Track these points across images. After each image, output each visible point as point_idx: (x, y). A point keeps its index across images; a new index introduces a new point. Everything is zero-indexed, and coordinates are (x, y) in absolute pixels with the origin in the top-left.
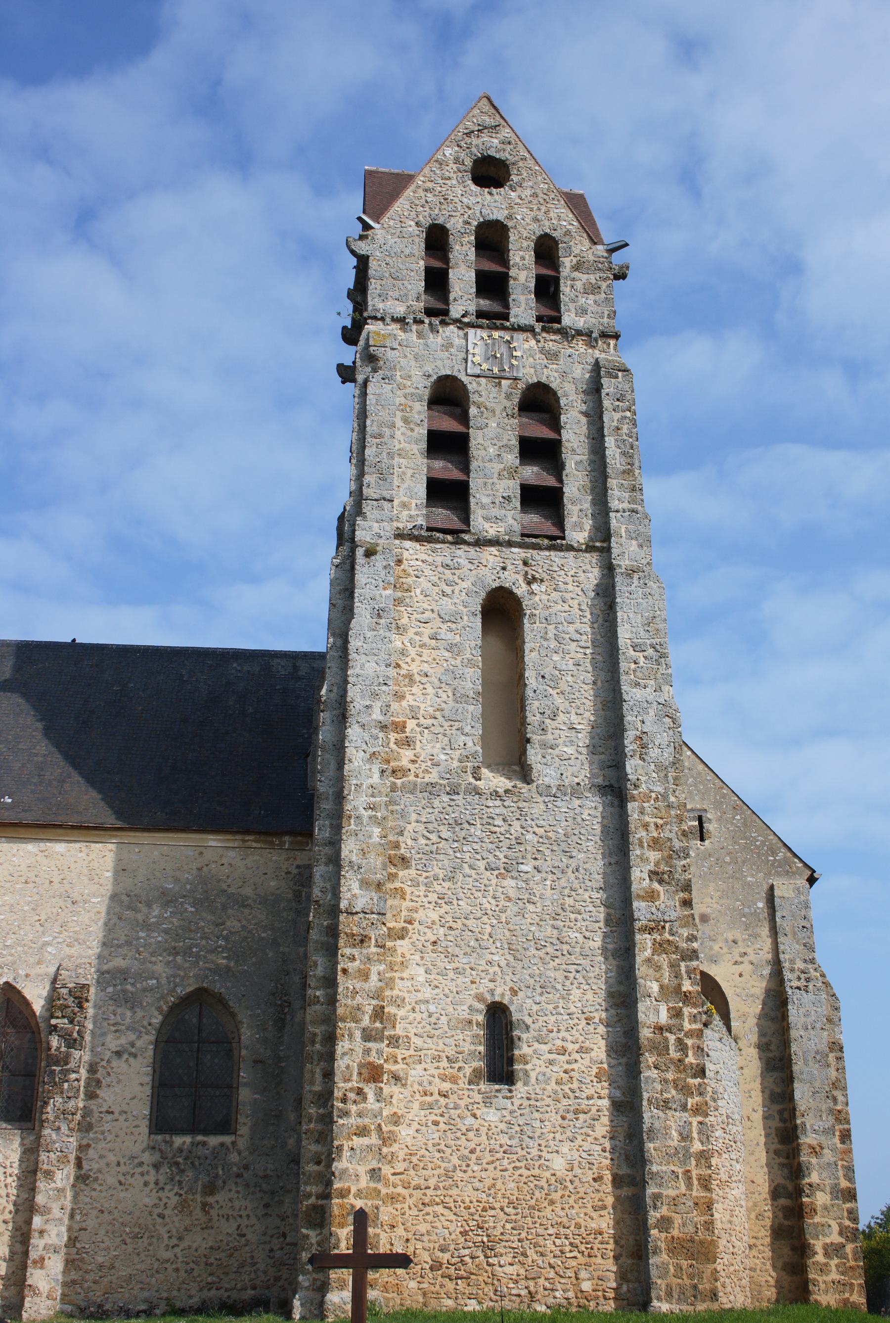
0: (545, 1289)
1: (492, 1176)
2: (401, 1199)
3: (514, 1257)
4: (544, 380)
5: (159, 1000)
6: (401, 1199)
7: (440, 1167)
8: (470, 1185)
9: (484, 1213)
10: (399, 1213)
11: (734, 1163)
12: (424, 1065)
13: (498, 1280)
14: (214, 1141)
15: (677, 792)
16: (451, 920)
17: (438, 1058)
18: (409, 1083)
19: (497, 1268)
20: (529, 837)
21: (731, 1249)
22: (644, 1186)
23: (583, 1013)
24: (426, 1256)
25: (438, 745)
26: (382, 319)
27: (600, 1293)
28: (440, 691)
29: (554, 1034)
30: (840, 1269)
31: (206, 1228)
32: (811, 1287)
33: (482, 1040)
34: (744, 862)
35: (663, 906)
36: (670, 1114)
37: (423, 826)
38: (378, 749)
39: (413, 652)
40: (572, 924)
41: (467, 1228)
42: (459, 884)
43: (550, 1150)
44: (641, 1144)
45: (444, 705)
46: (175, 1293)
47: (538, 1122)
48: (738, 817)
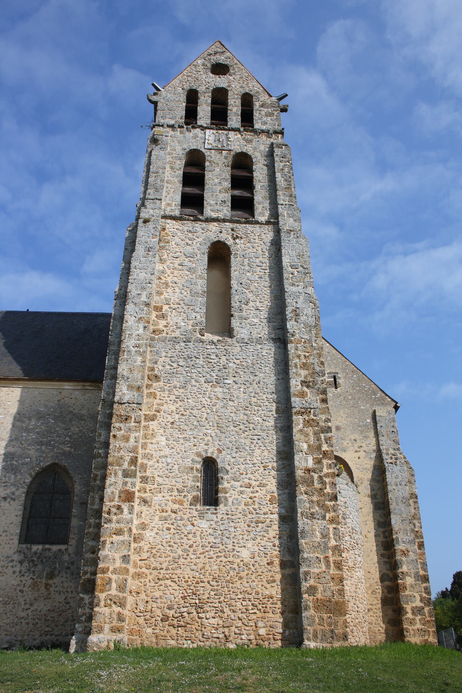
0: (235, 634)
1: (203, 561)
2: (144, 575)
3: (216, 613)
4: (244, 151)
5: (30, 469)
6: (144, 575)
7: (170, 556)
8: (188, 567)
9: (197, 585)
10: (143, 584)
11: (357, 556)
12: (162, 494)
13: (205, 628)
14: (55, 548)
15: (317, 342)
16: (183, 410)
17: (171, 490)
18: (153, 504)
19: (204, 620)
20: (231, 365)
21: (357, 609)
22: (299, 567)
23: (262, 463)
24: (158, 612)
25: (180, 318)
26: (162, 126)
27: (271, 636)
28: (183, 291)
29: (244, 475)
30: (422, 622)
31: (47, 598)
32: (405, 633)
33: (200, 480)
34: (359, 399)
35: (309, 400)
36: (315, 522)
37: (169, 359)
38: (143, 316)
39: (169, 272)
40: (256, 413)
41: (186, 594)
42: (189, 390)
43: (240, 546)
44: (297, 540)
45: (184, 298)
46: (26, 637)
47: (233, 528)
48: (355, 376)
